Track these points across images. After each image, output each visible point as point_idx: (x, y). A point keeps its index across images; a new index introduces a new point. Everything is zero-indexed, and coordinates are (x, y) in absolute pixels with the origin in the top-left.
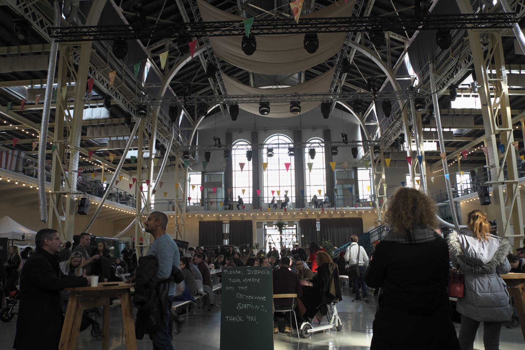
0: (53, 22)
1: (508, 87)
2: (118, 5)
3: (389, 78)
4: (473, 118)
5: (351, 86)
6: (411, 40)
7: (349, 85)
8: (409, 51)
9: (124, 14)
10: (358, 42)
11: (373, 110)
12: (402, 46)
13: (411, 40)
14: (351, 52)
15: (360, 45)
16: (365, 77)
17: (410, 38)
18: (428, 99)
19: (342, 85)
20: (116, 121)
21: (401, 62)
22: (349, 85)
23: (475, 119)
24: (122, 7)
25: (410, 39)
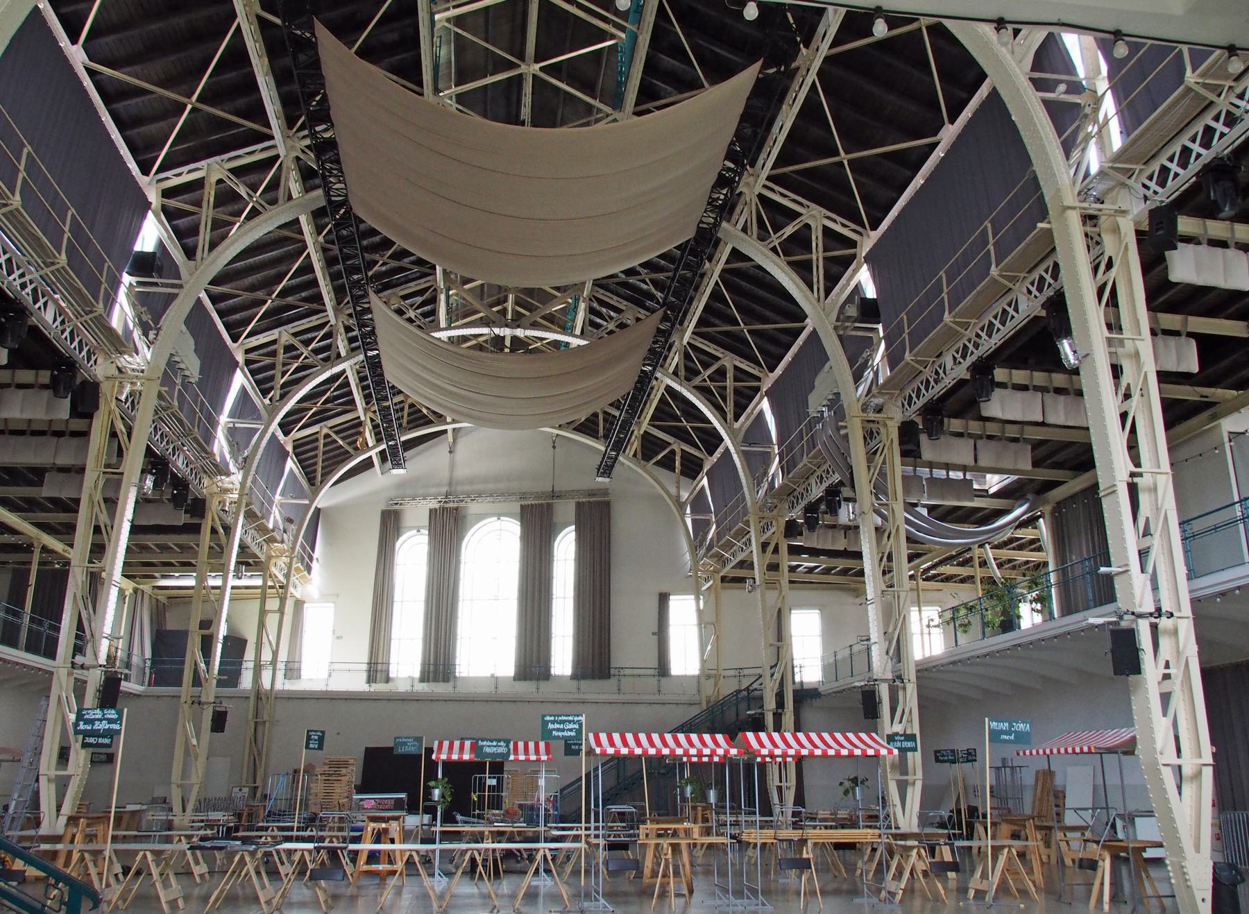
0: (209, 450)
1: (1183, 337)
2: (74, 41)
3: (727, 441)
4: (1029, 447)
5: (711, 348)
6: (875, 235)
7: (701, 344)
8: (867, 259)
9: (91, 72)
10: (671, 370)
11: (703, 486)
12: (756, 384)
13: (875, 235)
14: (702, 288)
15: (674, 377)
16: (745, 324)
17: (872, 230)
18: (910, 395)
19: (642, 432)
20: (26, 376)
21: (756, 412)
22: (701, 344)
23: (1033, 449)
24: (85, 47)
25: (770, 374)
